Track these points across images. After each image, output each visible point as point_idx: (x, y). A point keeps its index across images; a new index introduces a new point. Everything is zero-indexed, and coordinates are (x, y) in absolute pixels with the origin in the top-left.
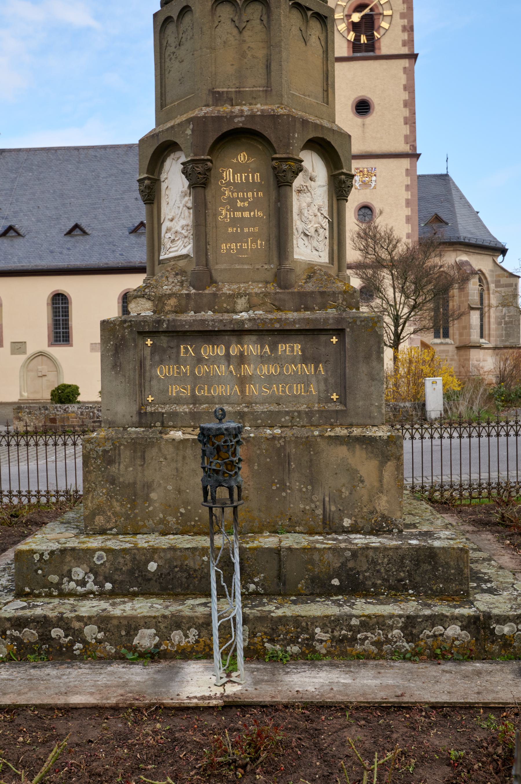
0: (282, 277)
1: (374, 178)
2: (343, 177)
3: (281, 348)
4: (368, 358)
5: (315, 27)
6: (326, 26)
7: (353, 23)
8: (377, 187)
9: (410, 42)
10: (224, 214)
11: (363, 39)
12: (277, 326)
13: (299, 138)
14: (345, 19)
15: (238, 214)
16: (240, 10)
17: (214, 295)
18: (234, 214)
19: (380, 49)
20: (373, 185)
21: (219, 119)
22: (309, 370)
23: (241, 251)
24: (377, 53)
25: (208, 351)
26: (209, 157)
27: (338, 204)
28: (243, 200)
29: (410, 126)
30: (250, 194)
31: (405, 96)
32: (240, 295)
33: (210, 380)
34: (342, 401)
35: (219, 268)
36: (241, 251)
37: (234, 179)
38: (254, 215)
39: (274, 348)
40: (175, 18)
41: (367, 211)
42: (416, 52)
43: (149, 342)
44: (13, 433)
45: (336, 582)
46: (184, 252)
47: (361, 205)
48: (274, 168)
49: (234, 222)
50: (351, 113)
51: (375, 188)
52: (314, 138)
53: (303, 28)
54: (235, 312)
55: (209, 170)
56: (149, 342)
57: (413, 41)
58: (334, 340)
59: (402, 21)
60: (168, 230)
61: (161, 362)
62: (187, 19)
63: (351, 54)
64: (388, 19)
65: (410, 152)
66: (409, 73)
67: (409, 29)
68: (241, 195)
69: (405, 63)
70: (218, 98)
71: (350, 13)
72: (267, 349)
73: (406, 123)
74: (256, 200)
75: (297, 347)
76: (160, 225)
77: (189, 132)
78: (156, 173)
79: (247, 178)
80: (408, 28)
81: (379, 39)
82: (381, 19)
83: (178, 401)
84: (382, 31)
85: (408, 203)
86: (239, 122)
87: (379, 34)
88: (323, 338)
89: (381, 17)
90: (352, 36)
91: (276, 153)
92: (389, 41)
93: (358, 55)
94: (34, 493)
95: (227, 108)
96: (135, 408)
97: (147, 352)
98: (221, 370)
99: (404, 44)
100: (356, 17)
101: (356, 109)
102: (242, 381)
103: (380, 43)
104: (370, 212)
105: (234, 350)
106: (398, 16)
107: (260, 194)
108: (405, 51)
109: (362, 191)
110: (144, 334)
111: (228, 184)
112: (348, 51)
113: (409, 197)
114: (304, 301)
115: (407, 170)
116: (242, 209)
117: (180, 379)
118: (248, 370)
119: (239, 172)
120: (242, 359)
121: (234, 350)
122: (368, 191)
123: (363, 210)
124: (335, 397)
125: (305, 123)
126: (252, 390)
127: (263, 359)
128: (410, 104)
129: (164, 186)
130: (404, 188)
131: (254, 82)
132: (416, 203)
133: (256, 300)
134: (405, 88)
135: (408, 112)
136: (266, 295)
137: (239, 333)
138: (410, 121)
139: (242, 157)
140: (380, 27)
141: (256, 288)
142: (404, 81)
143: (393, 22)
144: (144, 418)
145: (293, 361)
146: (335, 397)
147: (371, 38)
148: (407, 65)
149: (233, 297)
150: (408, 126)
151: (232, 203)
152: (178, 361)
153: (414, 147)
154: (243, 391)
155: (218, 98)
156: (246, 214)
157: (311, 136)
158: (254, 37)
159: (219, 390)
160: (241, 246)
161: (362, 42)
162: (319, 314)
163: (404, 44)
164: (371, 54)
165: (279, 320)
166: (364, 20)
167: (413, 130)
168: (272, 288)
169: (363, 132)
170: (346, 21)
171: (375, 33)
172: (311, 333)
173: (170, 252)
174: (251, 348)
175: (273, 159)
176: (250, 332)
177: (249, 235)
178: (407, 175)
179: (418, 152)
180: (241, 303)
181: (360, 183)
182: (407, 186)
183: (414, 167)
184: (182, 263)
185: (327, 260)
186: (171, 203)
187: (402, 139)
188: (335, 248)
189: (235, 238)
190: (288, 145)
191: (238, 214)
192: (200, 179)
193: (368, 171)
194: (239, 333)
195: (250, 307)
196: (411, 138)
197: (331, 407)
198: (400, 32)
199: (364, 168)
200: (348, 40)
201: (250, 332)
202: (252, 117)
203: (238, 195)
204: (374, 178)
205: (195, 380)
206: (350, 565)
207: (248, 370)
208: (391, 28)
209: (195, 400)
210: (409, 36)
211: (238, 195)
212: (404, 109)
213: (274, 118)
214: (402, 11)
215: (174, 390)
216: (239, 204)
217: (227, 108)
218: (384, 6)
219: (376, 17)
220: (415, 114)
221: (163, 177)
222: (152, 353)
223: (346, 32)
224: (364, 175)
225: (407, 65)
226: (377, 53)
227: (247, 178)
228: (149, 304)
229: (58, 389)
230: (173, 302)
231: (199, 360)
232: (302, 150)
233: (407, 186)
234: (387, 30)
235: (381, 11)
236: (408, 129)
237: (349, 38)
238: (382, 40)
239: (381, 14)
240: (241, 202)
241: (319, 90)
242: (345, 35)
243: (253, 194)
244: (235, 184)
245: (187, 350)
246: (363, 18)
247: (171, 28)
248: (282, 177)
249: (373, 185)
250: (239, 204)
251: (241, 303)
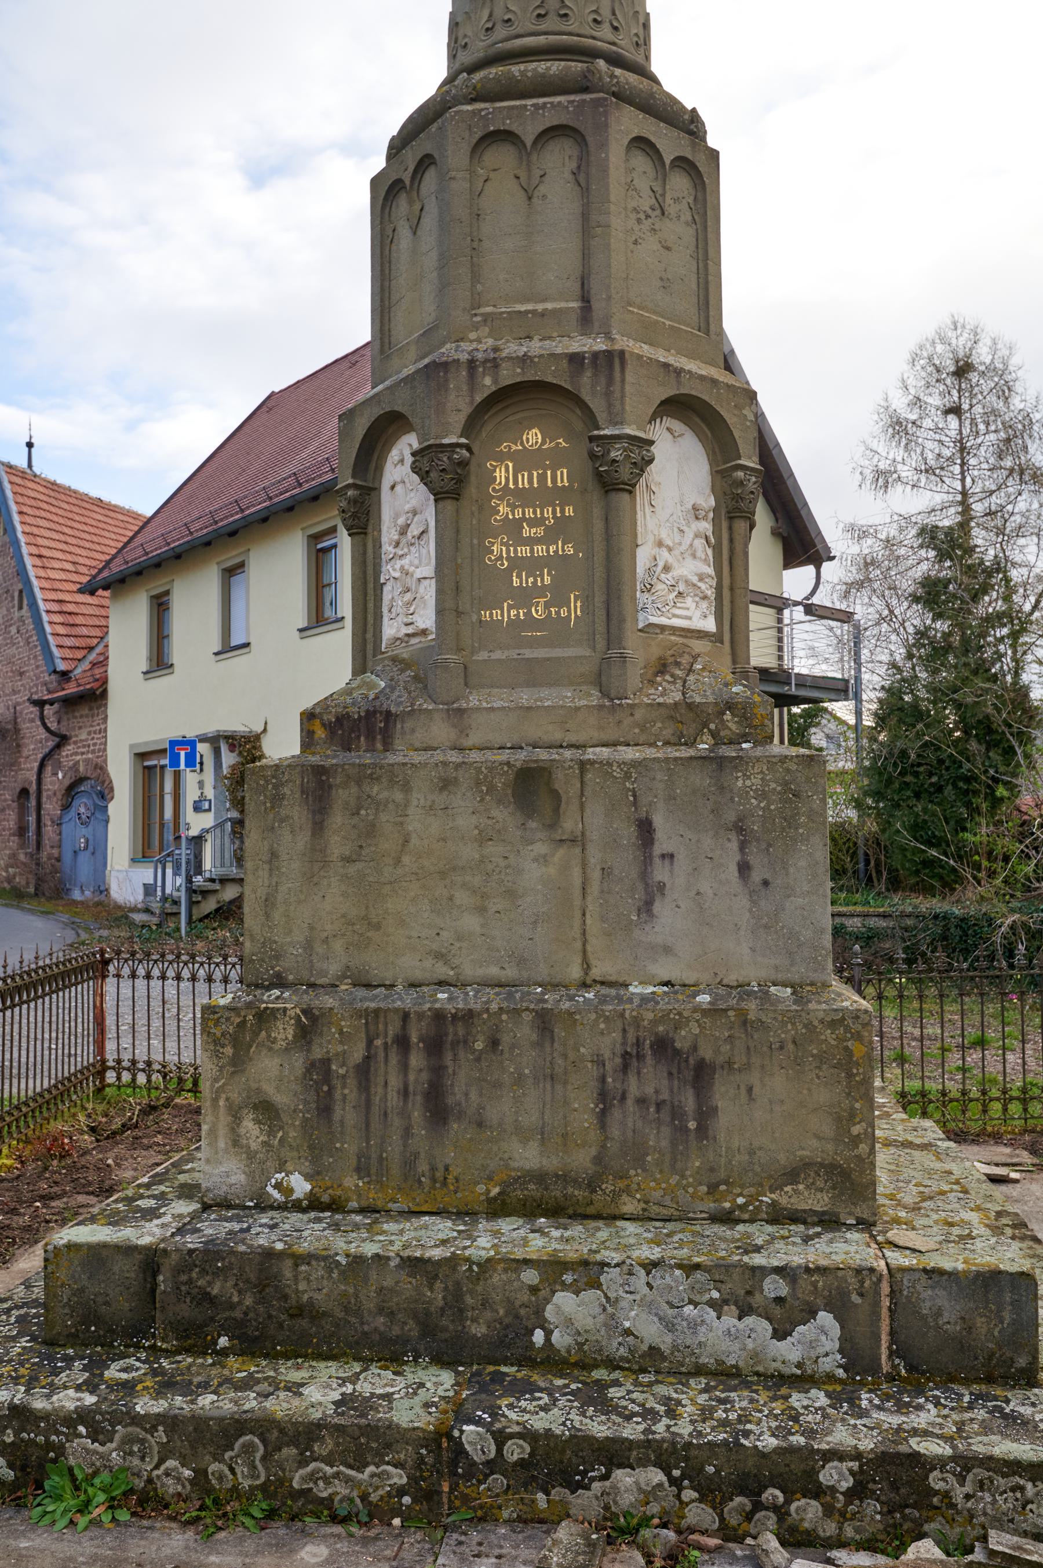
2: (740, 474)
5: (679, 183)
15: (524, 551)
16: (529, 154)
18: (516, 551)
26: (463, 440)
27: (730, 528)
28: (533, 523)
30: (548, 513)
37: (516, 482)
38: (556, 552)
40: (408, 183)
44: (955, 1094)
48: (593, 456)
49: (516, 563)
52: (675, 395)
53: (658, 189)
55: (464, 464)
68: (529, 513)
74: (562, 522)
78: (370, 475)
79: (542, 478)
91: (598, 428)
94: (141, 1065)
107: (569, 511)
116: (531, 542)
119: (527, 462)
139: (534, 437)
156: (540, 550)
157: (677, 154)
173: (675, 616)
175: (592, 439)
188: (371, 605)
191: (524, 551)
203: (524, 513)
211: (524, 513)
216: (527, 531)
227: (542, 478)
229: (112, 789)
232: (653, 419)
240: (530, 527)
243: (554, 512)
244: (518, 493)
247: (402, 205)
248: (613, 477)
250: (527, 531)
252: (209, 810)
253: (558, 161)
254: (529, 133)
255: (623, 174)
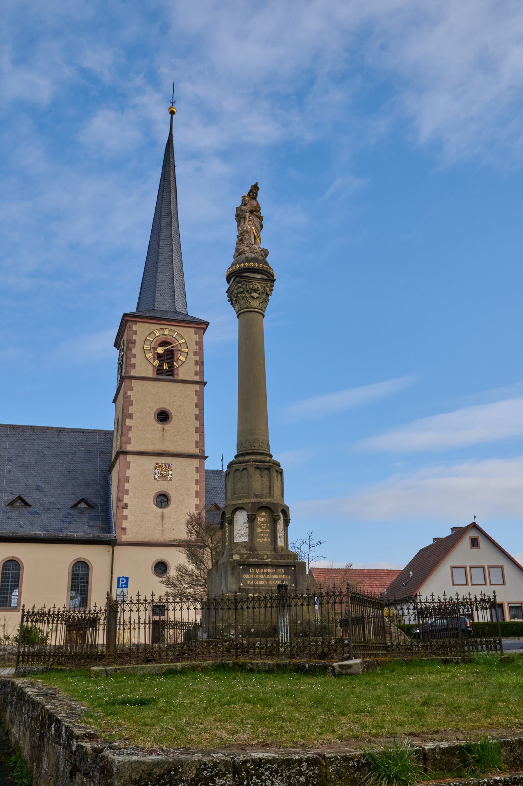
0: (275, 549)
1: (170, 472)
3: (278, 570)
4: (302, 574)
5: (279, 475)
6: (270, 473)
7: (158, 354)
8: (173, 479)
9: (200, 373)
10: (258, 530)
11: (165, 366)
12: (278, 564)
13: (280, 509)
14: (152, 350)
15: (262, 530)
17: (258, 554)
19: (178, 375)
20: (169, 478)
21: (258, 503)
22: (286, 577)
23: (263, 541)
24: (176, 377)
25: (258, 571)
28: (264, 526)
29: (200, 435)
31: (197, 412)
32: (265, 555)
33: (259, 579)
34: (296, 586)
35: (257, 545)
36: (263, 541)
39: (276, 570)
41: (163, 498)
42: (205, 381)
43: (241, 567)
45: (301, 635)
46: (246, 540)
47: (159, 494)
49: (261, 532)
50: (154, 419)
51: (171, 480)
54: (263, 559)
56: (241, 567)
57: (203, 372)
58: (293, 568)
59: (195, 357)
60: (238, 533)
61: (245, 573)
62: (245, 471)
63: (155, 376)
64: (185, 354)
65: (200, 454)
66: (200, 395)
67: (200, 363)
69: (197, 387)
70: (256, 496)
71: (156, 346)
72: (274, 570)
73: (196, 432)
74: (267, 526)
75: (283, 570)
76: (234, 531)
77: (250, 506)
80: (199, 363)
81: (177, 368)
82: (179, 354)
83: (249, 585)
84: (180, 363)
85: (197, 494)
86: (264, 504)
87: (178, 364)
88: (290, 568)
89: (180, 352)
90: (156, 363)
92: (185, 369)
93: (161, 377)
95: (259, 500)
96: (238, 587)
97: (241, 570)
98: (262, 576)
99: (196, 374)
100: (160, 350)
101: (158, 417)
102: (268, 580)
103: (178, 371)
104: (166, 500)
105: (265, 571)
106: (192, 353)
108: (197, 378)
109: (160, 482)
110: (240, 565)
111: (259, 521)
112: (153, 373)
113: (198, 490)
114: (282, 557)
115: (197, 468)
116: (264, 529)
117: (250, 579)
118: (269, 576)
120: (267, 573)
121: (265, 571)
122: (165, 482)
123: (160, 497)
124: (293, 585)
125: (281, 505)
126: (270, 582)
127: (273, 574)
128: (200, 418)
129: (235, 520)
130: (194, 482)
131: (266, 492)
132: (204, 495)
133: (269, 556)
134: (196, 406)
135: (198, 423)
136: (272, 555)
137: (267, 565)
138: (200, 430)
140: (178, 359)
141: (269, 553)
142: (195, 400)
143: (188, 357)
144: (240, 590)
145: (282, 574)
146: (293, 585)
147: (171, 366)
148: (198, 389)
149: (263, 555)
150: (198, 434)
151: (260, 527)
152: (249, 573)
153: (203, 451)
154: (268, 583)
155: (256, 496)
156: (265, 530)
158: (266, 479)
159: (261, 583)
160: (263, 539)
161: (164, 368)
162: (287, 561)
163: (196, 374)
164: (171, 378)
165: (278, 562)
166: (166, 353)
167: (202, 437)
168: (273, 553)
169: (163, 435)
170: (152, 352)
171: (175, 363)
172: (286, 566)
174: (270, 570)
176: (270, 565)
177: (266, 536)
178: (197, 472)
179: (206, 455)
180: (265, 557)
181: (159, 475)
182: (197, 481)
183: (202, 465)
184: (243, 544)
185: (283, 545)
186: (239, 525)
187: (194, 444)
189: (262, 537)
190: (278, 512)
191: (262, 530)
192: (251, 520)
193: (166, 466)
194: (267, 565)
195: (268, 558)
196: (200, 444)
197: (292, 588)
198: (194, 365)
199: (162, 464)
200: (153, 366)
201: (270, 565)
202: (268, 503)
204: (170, 472)
205: (254, 579)
206: (305, 630)
207: (269, 576)
208: (186, 361)
209: (254, 585)
210: (200, 368)
212: (195, 421)
213: (274, 504)
214: (195, 350)
215: (248, 582)
217: (259, 500)
218: (182, 345)
219: (175, 352)
220: (204, 425)
221: (235, 516)
222: (242, 571)
223: (152, 359)
224: (162, 469)
225: (198, 389)
226: (176, 377)
228: (239, 556)
230: (246, 556)
231: (255, 573)
233: (197, 481)
234: (184, 362)
235: (180, 348)
236: (198, 436)
237: (154, 364)
238: (179, 368)
239: (179, 350)
241: (280, 493)
242: (152, 362)
245: (252, 570)
246: (165, 350)
247: (238, 472)
248: (274, 521)
249: (169, 478)
251: (265, 557)
252: (119, 578)
253: (266, 472)
254: (241, 469)
255: (275, 474)
